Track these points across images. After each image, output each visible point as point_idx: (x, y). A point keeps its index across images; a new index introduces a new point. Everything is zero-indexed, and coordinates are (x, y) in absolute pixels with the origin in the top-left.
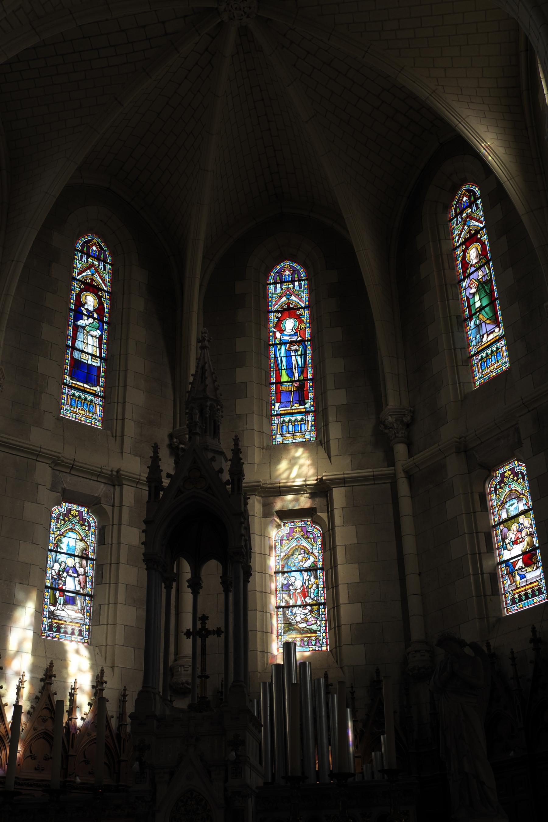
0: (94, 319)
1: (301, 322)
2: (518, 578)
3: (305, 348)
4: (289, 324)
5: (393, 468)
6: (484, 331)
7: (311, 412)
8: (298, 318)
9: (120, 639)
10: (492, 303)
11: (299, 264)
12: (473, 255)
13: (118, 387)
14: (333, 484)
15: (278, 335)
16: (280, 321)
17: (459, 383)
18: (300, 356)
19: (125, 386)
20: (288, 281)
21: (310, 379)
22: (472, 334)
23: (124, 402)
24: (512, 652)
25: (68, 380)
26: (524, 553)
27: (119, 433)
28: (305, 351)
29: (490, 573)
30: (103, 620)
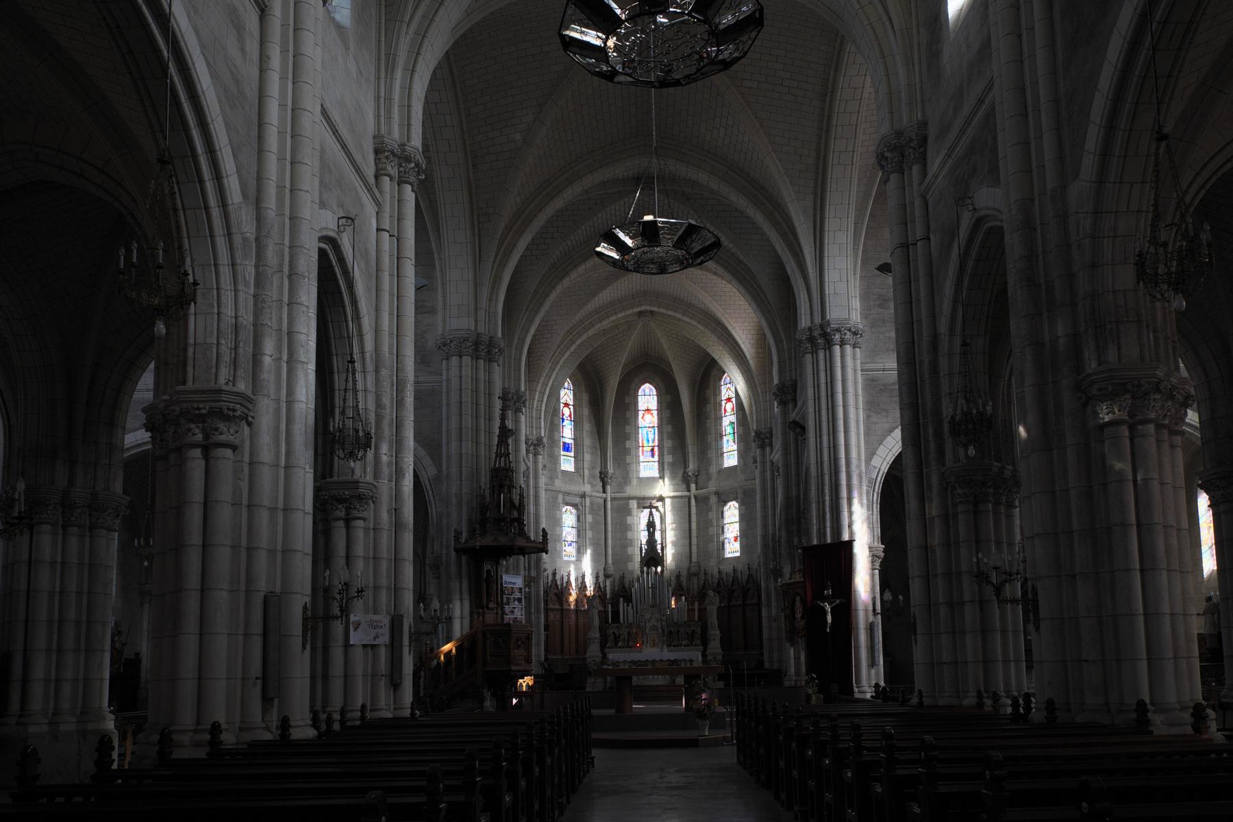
3: (654, 430)
4: (648, 416)
8: (652, 414)
10: (734, 433)
12: (729, 406)
19: (583, 453)
23: (583, 461)
25: (562, 453)
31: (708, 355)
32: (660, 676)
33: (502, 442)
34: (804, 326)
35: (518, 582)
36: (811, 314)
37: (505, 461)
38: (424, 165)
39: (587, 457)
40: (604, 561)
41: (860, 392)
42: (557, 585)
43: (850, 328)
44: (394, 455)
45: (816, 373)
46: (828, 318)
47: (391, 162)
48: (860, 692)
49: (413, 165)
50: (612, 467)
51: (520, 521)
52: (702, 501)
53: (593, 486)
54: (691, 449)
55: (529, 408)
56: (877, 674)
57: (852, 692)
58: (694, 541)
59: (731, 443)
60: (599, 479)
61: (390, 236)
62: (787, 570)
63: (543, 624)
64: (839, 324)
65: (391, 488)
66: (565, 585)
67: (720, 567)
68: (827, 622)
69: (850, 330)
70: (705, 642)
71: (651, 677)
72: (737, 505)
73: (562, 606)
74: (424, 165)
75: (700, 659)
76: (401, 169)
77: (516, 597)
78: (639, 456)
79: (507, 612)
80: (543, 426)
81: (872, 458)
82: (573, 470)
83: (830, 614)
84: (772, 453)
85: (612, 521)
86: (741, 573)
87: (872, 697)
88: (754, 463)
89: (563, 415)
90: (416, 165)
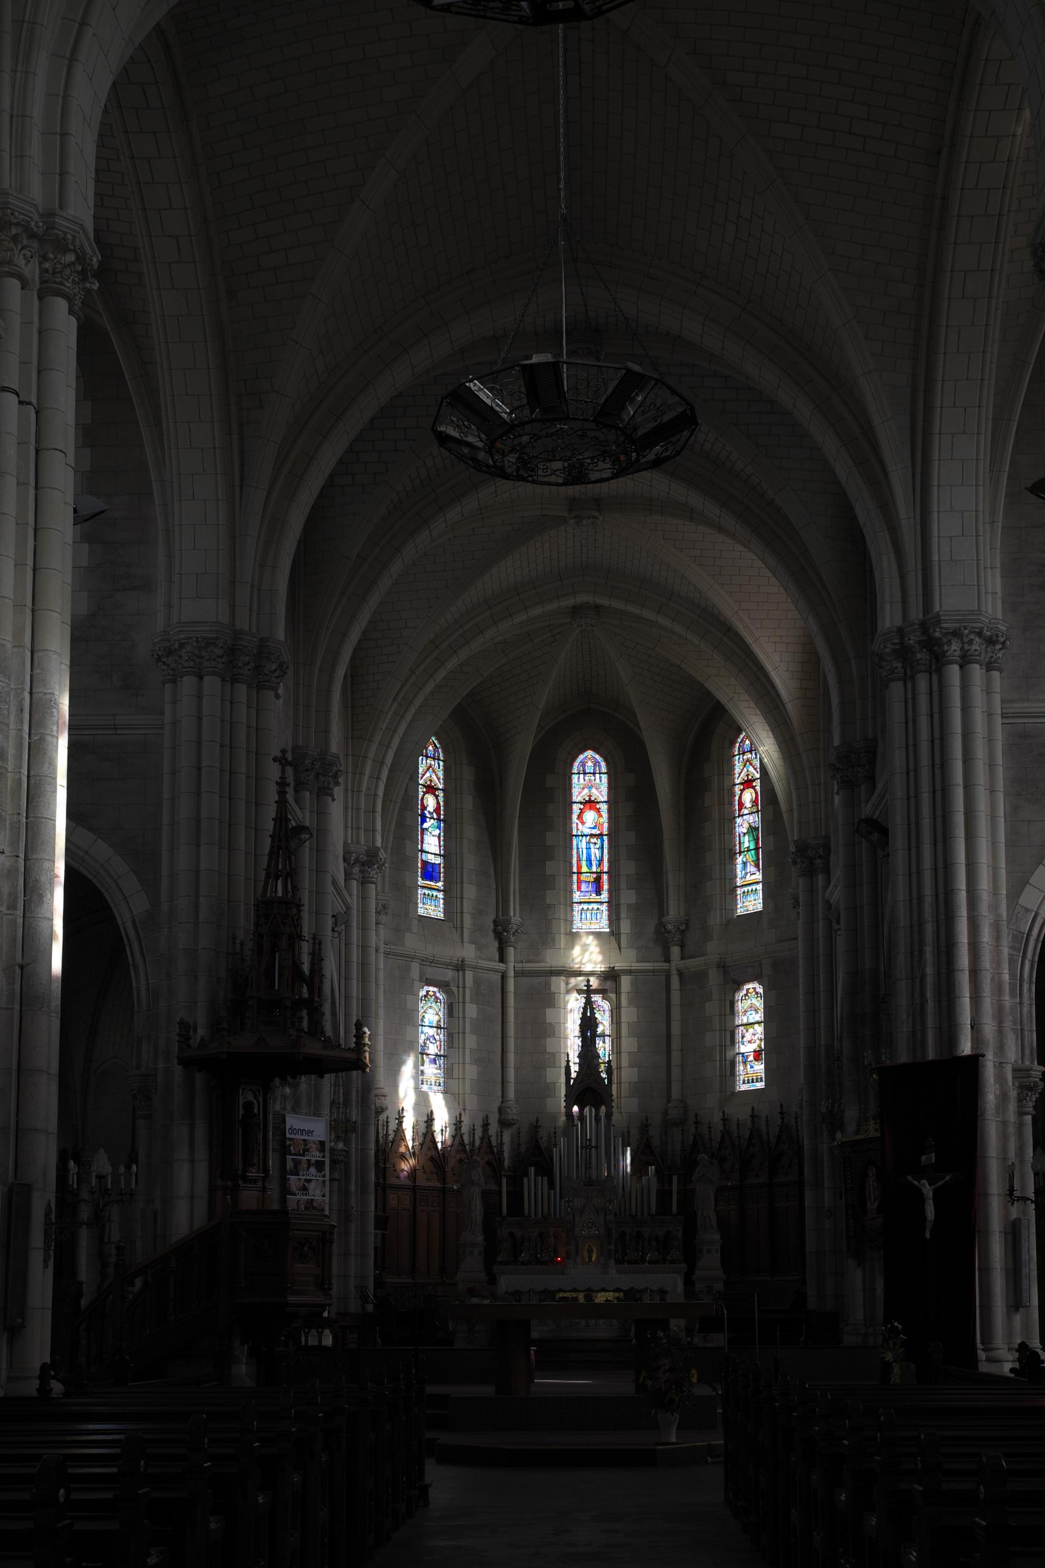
0: (434, 819)
1: (600, 816)
2: (748, 1067)
4: (590, 816)
5: (668, 964)
6: (748, 871)
7: (606, 902)
8: (598, 811)
9: (468, 1090)
10: (757, 849)
11: (601, 755)
12: (748, 796)
13: (456, 883)
14: (622, 973)
15: (580, 826)
16: (582, 812)
17: (725, 909)
18: (599, 849)
19: (462, 883)
20: (590, 773)
21: (605, 873)
22: (739, 867)
23: (462, 898)
24: (738, 1120)
25: (421, 882)
26: (755, 1051)
27: (459, 925)
28: (603, 845)
29: (731, 1061)
30: (455, 1075)
31: (709, 694)
32: (601, 1321)
33: (280, 848)
34: (887, 624)
35: (318, 1129)
36: (904, 602)
37: (285, 887)
38: (95, 259)
39: (470, 892)
40: (500, 1094)
41: (999, 759)
42: (490, 1145)
43: (982, 629)
44: (22, 856)
45: (911, 722)
46: (937, 609)
47: (23, 248)
48: (991, 1360)
49: (71, 257)
50: (518, 911)
51: (314, 1008)
52: (692, 980)
53: (479, 947)
54: (673, 879)
55: (353, 791)
56: (1026, 1325)
57: (974, 1360)
58: (676, 1057)
59: (751, 868)
60: (492, 935)
61: (21, 402)
62: (851, 1114)
63: (372, 1214)
64: (958, 621)
65: (14, 922)
66: (391, 1138)
67: (726, 1110)
68: (925, 1218)
69: (980, 634)
70: (691, 1256)
71: (583, 1322)
72: (760, 990)
73: (444, 1183)
74: (95, 259)
75: (680, 1287)
76: (47, 265)
77: (313, 1159)
78: (571, 892)
79: (294, 1189)
80: (379, 827)
81: (1023, 890)
82: (441, 916)
83: (931, 1202)
84: (827, 888)
85: (516, 1016)
86: (767, 1121)
87: (1012, 1370)
88: (795, 907)
89: (424, 808)
90: (78, 258)
